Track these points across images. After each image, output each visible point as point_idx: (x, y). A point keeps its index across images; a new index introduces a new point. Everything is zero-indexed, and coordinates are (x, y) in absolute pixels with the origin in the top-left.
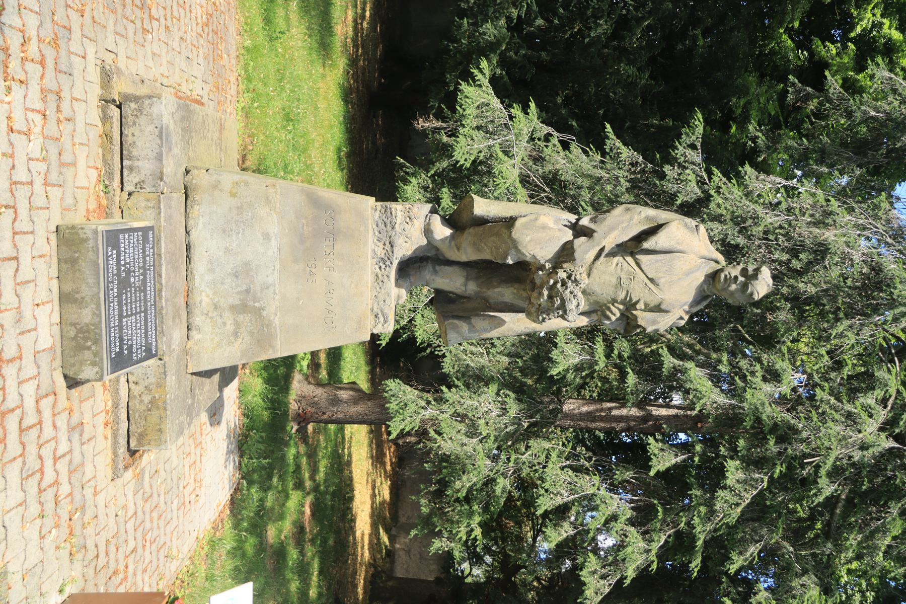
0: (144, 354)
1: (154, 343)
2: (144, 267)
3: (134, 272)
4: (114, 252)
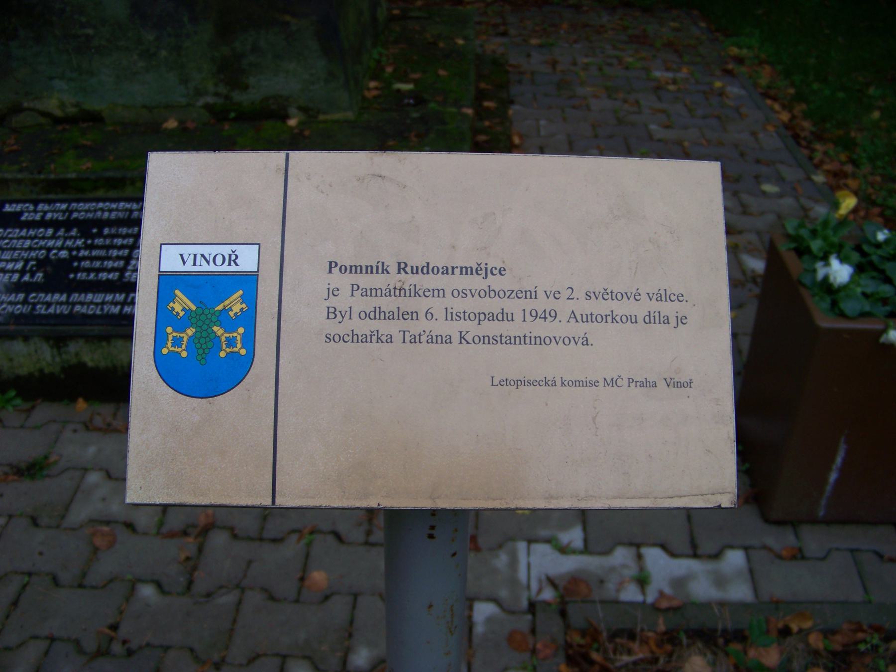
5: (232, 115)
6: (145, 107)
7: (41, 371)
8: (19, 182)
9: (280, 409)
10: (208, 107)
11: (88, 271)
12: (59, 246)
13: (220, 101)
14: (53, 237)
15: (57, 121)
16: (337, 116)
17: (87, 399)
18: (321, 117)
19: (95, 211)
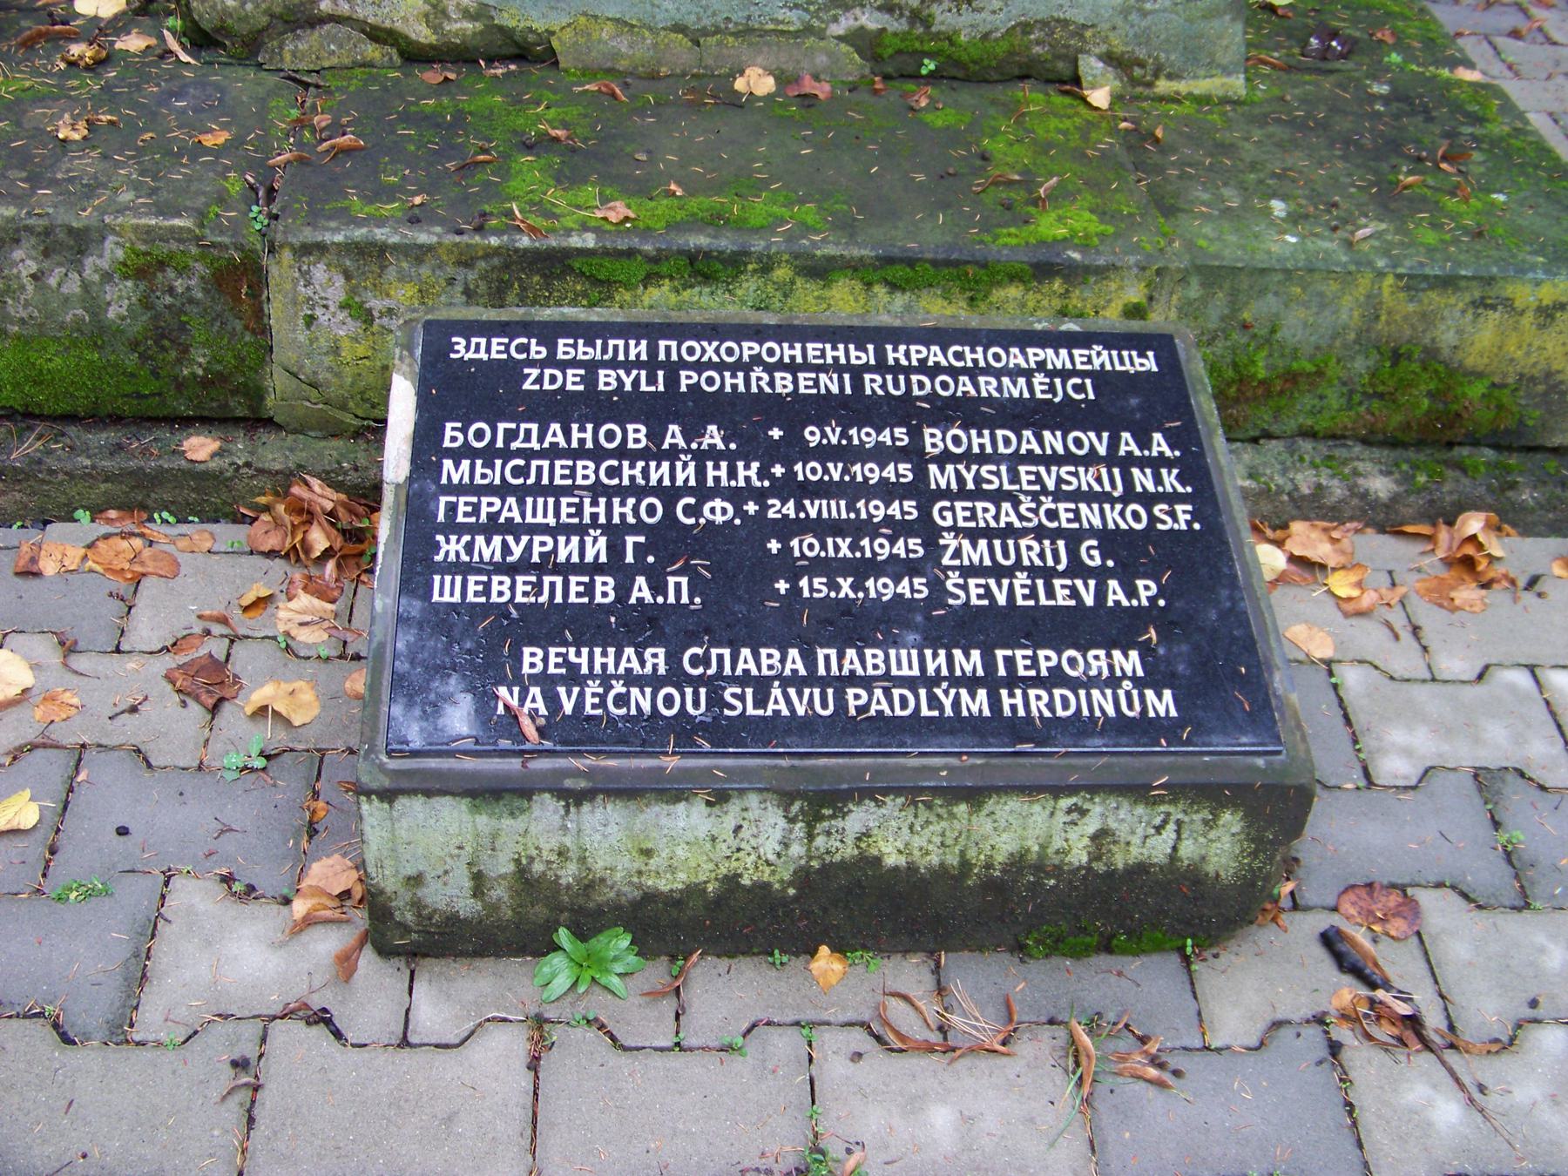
0: (1159, 444)
1: (1102, 358)
2: (655, 412)
3: (670, 495)
4: (531, 658)
5: (930, 66)
6: (679, 28)
7: (732, 880)
8: (419, 253)
9: (1423, 964)
10: (860, 40)
11: (829, 568)
12: (714, 483)
13: (895, 25)
14: (654, 453)
15: (414, 55)
16: (1202, 86)
17: (839, 949)
18: (1163, 86)
19: (747, 368)
